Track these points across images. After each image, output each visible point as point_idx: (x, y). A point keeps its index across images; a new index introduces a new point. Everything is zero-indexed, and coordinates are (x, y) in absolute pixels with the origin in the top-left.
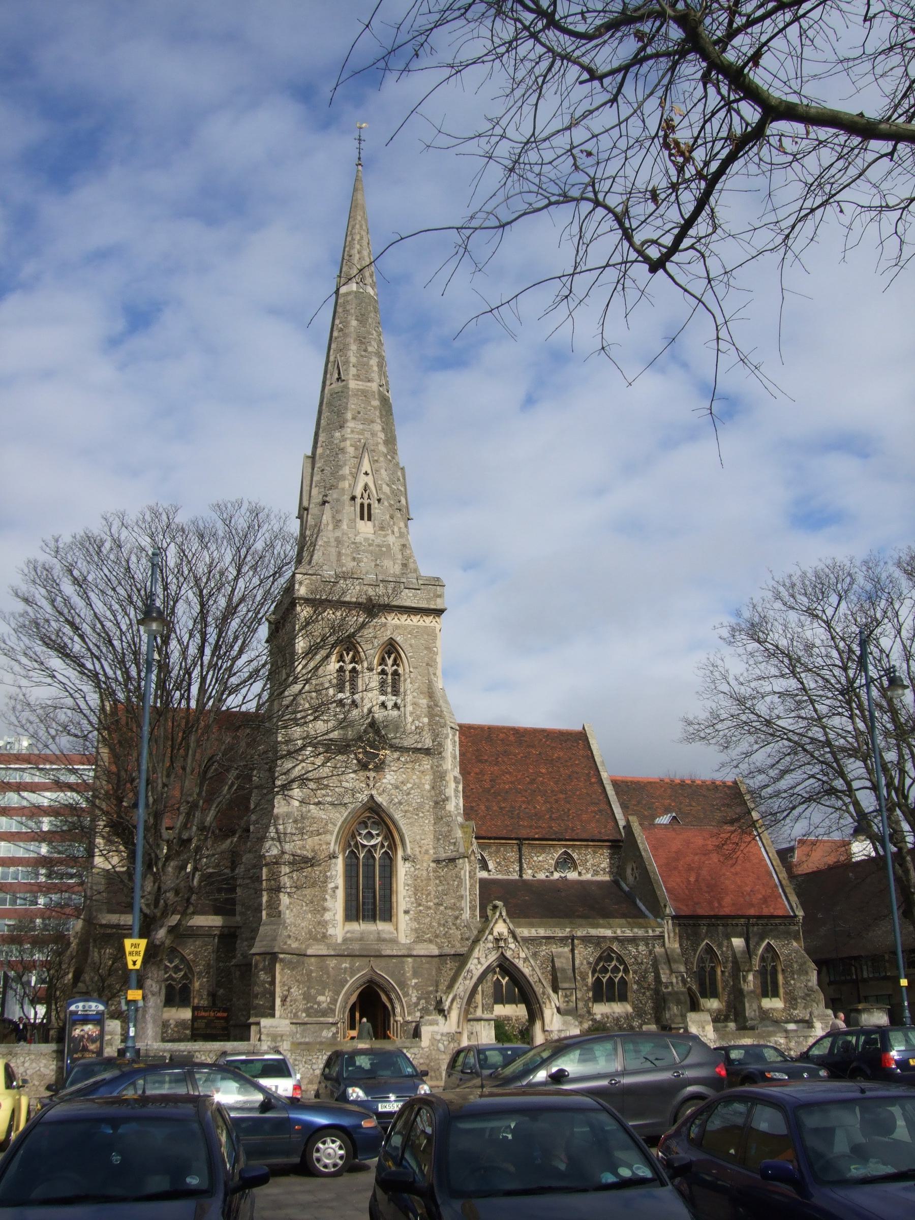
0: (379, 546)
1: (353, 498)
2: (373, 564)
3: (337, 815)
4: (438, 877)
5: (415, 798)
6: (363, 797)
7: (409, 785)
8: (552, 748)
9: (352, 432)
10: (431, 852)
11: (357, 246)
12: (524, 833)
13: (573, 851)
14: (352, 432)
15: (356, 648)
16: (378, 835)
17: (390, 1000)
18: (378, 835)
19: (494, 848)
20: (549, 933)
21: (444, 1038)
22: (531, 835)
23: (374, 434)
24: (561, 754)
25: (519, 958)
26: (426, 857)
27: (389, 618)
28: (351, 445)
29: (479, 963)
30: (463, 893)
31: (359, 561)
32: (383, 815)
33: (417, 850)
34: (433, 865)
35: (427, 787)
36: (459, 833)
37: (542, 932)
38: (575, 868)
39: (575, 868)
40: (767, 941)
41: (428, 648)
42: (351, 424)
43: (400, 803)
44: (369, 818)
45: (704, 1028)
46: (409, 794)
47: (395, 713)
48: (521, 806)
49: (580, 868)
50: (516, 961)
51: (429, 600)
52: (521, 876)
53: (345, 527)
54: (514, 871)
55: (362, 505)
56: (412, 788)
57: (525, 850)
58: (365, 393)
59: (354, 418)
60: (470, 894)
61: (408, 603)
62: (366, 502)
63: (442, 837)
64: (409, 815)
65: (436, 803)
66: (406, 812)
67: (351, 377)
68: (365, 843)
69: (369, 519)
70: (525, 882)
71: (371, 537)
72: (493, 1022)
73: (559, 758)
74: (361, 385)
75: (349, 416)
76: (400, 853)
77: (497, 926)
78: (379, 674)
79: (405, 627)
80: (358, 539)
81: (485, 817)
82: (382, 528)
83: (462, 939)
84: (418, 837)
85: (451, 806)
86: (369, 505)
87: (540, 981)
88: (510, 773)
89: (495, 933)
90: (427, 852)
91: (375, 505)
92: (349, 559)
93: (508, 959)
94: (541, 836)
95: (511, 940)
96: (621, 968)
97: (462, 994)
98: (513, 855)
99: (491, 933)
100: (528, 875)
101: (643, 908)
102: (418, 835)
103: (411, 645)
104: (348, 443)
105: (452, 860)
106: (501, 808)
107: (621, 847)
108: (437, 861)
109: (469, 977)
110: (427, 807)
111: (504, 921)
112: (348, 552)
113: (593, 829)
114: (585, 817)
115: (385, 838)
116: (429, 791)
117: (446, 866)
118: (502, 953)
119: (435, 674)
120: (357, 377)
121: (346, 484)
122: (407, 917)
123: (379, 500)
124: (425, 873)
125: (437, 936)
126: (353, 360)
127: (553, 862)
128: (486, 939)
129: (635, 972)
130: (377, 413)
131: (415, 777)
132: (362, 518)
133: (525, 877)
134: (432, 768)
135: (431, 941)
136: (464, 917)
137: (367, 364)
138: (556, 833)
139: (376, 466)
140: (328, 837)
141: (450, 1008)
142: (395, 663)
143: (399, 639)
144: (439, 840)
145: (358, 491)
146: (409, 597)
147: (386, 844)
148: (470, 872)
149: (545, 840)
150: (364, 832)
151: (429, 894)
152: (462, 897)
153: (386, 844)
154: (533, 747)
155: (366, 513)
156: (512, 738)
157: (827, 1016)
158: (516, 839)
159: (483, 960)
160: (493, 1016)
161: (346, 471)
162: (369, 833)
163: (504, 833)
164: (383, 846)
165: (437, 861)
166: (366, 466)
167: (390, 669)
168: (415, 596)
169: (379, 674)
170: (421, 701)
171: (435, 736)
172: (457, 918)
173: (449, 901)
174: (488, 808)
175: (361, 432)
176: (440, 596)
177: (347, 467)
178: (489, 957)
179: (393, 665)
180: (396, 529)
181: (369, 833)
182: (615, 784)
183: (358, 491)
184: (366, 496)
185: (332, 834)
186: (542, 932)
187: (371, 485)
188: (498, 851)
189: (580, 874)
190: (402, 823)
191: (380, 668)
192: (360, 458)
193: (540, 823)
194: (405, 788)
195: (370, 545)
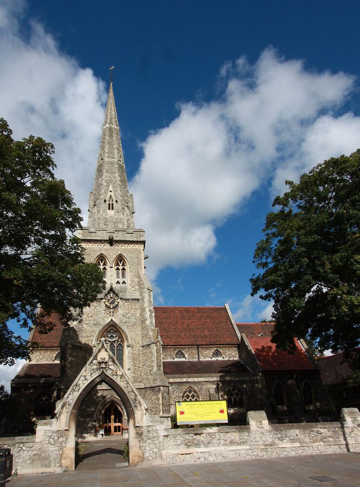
0: (116, 219)
1: (105, 201)
2: (113, 226)
3: (97, 328)
4: (143, 354)
5: (133, 320)
6: (108, 320)
7: (130, 315)
8: (212, 313)
9: (106, 177)
10: (140, 343)
11: (110, 111)
13: (220, 349)
14: (106, 177)
15: (105, 259)
16: (116, 336)
17: (122, 409)
18: (116, 336)
19: (187, 350)
20: (207, 379)
21: (55, 435)
24: (216, 315)
25: (117, 375)
26: (138, 345)
27: (120, 246)
28: (105, 182)
29: (85, 379)
30: (153, 359)
32: (117, 327)
33: (134, 342)
34: (141, 348)
35: (138, 315)
36: (151, 333)
37: (203, 379)
38: (221, 356)
39: (221, 356)
40: (305, 381)
41: (137, 257)
42: (105, 174)
43: (126, 323)
44: (112, 329)
45: (261, 422)
46: (129, 318)
47: (124, 285)
48: (198, 334)
49: (223, 356)
50: (114, 378)
51: (137, 238)
52: (199, 359)
53: (101, 212)
55: (109, 204)
56: (131, 316)
57: (200, 350)
58: (111, 163)
60: (157, 360)
62: (111, 203)
63: (145, 336)
64: (130, 327)
65: (142, 321)
66: (128, 326)
67: (106, 157)
68: (110, 340)
69: (113, 209)
70: (200, 362)
72: (170, 418)
73: (215, 316)
74: (110, 160)
75: (104, 171)
76: (126, 344)
77: (100, 354)
78: (116, 270)
79: (127, 250)
80: (107, 217)
81: (183, 338)
82: (118, 212)
83: (153, 380)
84: (134, 337)
85: (148, 322)
86: (112, 204)
87: (133, 391)
89: (99, 359)
90: (138, 343)
91: (114, 203)
92: (103, 224)
93: (108, 376)
94: (206, 344)
95: (110, 363)
96: (240, 393)
97: (71, 402)
99: (96, 358)
100: (202, 359)
101: (249, 369)
102: (134, 336)
103: (130, 257)
104: (104, 181)
105: (149, 345)
106: (191, 335)
107: (241, 346)
108: (143, 347)
109: (77, 389)
110: (138, 324)
112: (102, 222)
113: (228, 340)
114: (225, 336)
115: (119, 338)
116: (139, 317)
117: (146, 348)
118: (103, 372)
119: (141, 268)
120: (108, 157)
121: (102, 196)
122: (129, 372)
123: (117, 201)
124: (137, 352)
125: (143, 380)
126: (107, 151)
127: (212, 354)
128: (91, 363)
129: (246, 395)
130: (117, 169)
131: (132, 311)
132: (109, 209)
133: (200, 360)
134: (140, 307)
135: (141, 382)
136: (154, 370)
137: (113, 152)
138: (212, 342)
139: (116, 189)
140: (92, 338)
141: (61, 413)
142: (123, 265)
144: (143, 337)
145: (107, 199)
147: (120, 340)
148: (156, 350)
149: (208, 345)
150: (110, 336)
151: (140, 361)
152: (153, 361)
153: (120, 340)
154: (204, 313)
155: (111, 207)
156: (196, 310)
157: (355, 413)
159: (88, 377)
160: (170, 415)
161: (103, 191)
162: (112, 336)
163: (191, 343)
164: (118, 341)
165: (143, 347)
166: (111, 188)
167: (121, 268)
168: (131, 236)
169: (116, 270)
171: (141, 293)
172: (151, 371)
173: (148, 363)
174: (185, 335)
175: (110, 177)
176: (142, 236)
177: (103, 191)
178: (93, 375)
179: (122, 266)
180: (125, 213)
181: (112, 336)
182: (238, 326)
183: (107, 199)
184: (111, 200)
185: (94, 337)
186: (203, 379)
187: (113, 196)
189: (223, 358)
190: (126, 331)
192: (108, 186)
193: (206, 339)
194: (128, 316)
195: (112, 219)
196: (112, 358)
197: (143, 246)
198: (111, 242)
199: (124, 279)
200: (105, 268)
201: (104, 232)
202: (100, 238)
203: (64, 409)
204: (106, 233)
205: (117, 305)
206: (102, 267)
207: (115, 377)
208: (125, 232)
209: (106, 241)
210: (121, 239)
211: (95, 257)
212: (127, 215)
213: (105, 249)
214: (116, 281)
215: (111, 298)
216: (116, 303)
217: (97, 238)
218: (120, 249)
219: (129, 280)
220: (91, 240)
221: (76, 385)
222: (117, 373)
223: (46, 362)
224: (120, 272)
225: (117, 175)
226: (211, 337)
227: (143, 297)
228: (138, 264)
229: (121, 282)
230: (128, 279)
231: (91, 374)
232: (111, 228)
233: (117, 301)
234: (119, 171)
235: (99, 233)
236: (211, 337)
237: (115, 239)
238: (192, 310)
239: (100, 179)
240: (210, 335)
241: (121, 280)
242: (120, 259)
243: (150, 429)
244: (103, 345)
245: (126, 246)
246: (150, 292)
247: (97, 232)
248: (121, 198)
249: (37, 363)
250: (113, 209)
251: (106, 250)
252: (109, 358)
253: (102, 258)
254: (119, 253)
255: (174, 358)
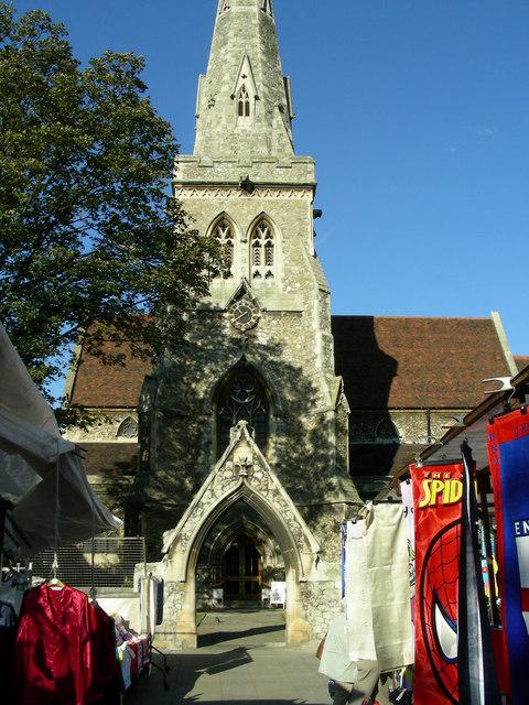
2: (249, 151)
12: (431, 403)
22: (438, 405)
23: (254, 46)
25: (267, 490)
31: (236, 150)
41: (299, 219)
54: (423, 437)
55: (241, 103)
58: (246, 15)
59: (236, 35)
61: (280, 180)
62: (244, 100)
71: (248, 128)
77: (238, 450)
80: (236, 131)
86: (247, 103)
87: (295, 520)
88: (422, 354)
89: (236, 460)
98: (422, 423)
109: (199, 513)
111: (249, 445)
118: (243, 483)
132: (240, 114)
142: (269, 235)
143: (271, 214)
146: (280, 175)
156: (427, 326)
158: (424, 409)
163: (413, 404)
167: (263, 242)
169: (254, 246)
170: (293, 268)
175: (242, 45)
180: (274, 122)
184: (244, 95)
188: (408, 419)
191: (254, 241)
196: (259, 459)
197: (311, 194)
198: (248, 187)
199: (268, 268)
200: (229, 243)
201: (230, 165)
202: (222, 180)
203: (179, 545)
204: (233, 167)
205: (256, 325)
206: (223, 240)
207: (265, 493)
208: (274, 165)
209: (233, 185)
210: (266, 180)
211: (210, 219)
212: (279, 127)
213: (231, 202)
214: (253, 272)
215: (243, 309)
216: (253, 321)
217: (216, 179)
218: (262, 201)
219: (279, 270)
220: (203, 183)
221: (197, 506)
222: (267, 485)
223: (100, 440)
224: (262, 250)
225: (257, 40)
226: (457, 390)
227: (311, 307)
228: (299, 234)
229: (263, 273)
230: (278, 266)
231: (223, 486)
232: (244, 153)
233: (254, 315)
234: (261, 33)
235: (218, 168)
236: (457, 390)
237: (257, 180)
238: (418, 325)
239: (223, 51)
240: (458, 384)
241: (263, 269)
242: (261, 224)
243: (325, 587)
244: (243, 434)
245: (273, 196)
246: (325, 297)
247: (216, 165)
248: (266, 90)
249: (82, 441)
250: (247, 114)
251: (234, 204)
252: (254, 458)
253: (221, 222)
254: (261, 209)
255: (374, 439)
